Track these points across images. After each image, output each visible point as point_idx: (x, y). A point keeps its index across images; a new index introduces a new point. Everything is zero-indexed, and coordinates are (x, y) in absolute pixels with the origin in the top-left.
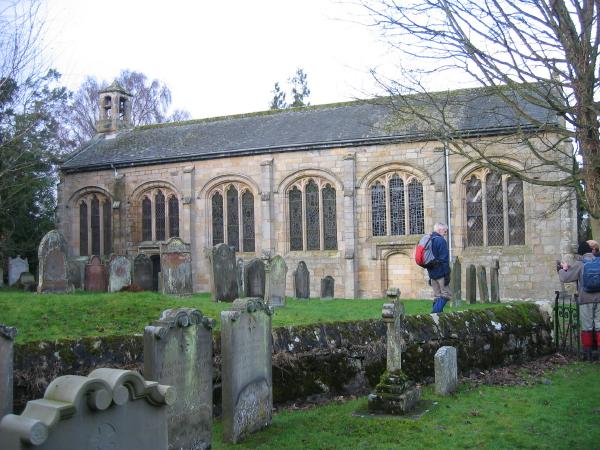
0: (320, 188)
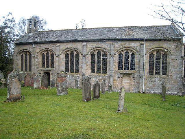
0: (102, 54)
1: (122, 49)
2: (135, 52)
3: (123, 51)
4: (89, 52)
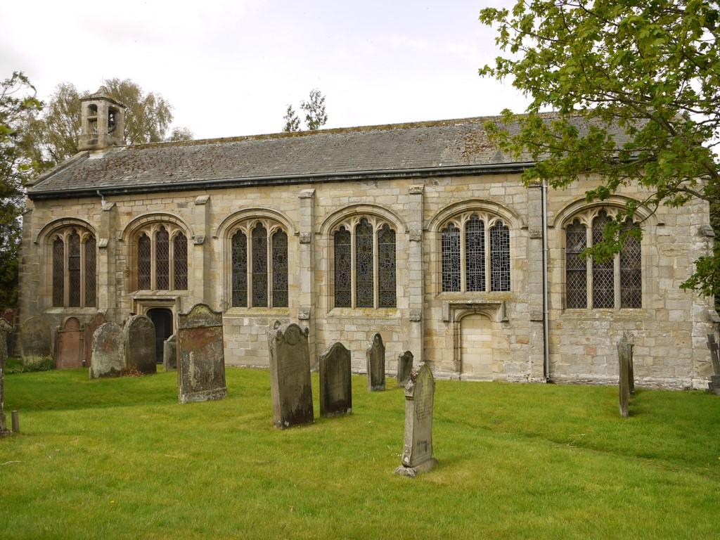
0: (375, 229)
1: (455, 210)
2: (508, 220)
3: (457, 216)
4: (324, 224)
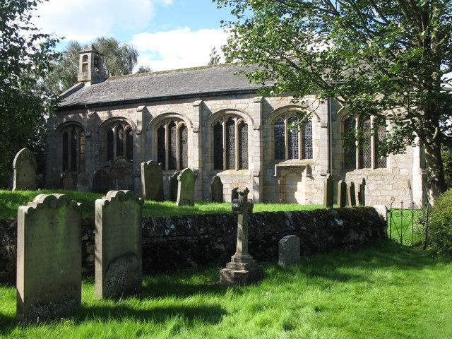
0: (236, 123)
